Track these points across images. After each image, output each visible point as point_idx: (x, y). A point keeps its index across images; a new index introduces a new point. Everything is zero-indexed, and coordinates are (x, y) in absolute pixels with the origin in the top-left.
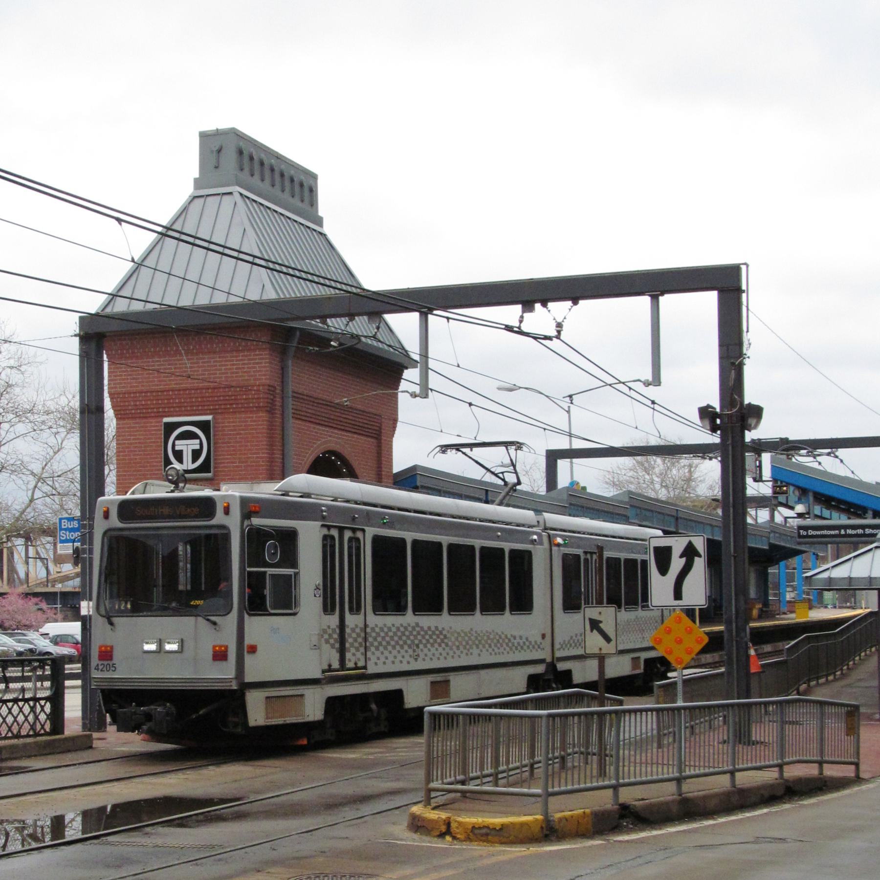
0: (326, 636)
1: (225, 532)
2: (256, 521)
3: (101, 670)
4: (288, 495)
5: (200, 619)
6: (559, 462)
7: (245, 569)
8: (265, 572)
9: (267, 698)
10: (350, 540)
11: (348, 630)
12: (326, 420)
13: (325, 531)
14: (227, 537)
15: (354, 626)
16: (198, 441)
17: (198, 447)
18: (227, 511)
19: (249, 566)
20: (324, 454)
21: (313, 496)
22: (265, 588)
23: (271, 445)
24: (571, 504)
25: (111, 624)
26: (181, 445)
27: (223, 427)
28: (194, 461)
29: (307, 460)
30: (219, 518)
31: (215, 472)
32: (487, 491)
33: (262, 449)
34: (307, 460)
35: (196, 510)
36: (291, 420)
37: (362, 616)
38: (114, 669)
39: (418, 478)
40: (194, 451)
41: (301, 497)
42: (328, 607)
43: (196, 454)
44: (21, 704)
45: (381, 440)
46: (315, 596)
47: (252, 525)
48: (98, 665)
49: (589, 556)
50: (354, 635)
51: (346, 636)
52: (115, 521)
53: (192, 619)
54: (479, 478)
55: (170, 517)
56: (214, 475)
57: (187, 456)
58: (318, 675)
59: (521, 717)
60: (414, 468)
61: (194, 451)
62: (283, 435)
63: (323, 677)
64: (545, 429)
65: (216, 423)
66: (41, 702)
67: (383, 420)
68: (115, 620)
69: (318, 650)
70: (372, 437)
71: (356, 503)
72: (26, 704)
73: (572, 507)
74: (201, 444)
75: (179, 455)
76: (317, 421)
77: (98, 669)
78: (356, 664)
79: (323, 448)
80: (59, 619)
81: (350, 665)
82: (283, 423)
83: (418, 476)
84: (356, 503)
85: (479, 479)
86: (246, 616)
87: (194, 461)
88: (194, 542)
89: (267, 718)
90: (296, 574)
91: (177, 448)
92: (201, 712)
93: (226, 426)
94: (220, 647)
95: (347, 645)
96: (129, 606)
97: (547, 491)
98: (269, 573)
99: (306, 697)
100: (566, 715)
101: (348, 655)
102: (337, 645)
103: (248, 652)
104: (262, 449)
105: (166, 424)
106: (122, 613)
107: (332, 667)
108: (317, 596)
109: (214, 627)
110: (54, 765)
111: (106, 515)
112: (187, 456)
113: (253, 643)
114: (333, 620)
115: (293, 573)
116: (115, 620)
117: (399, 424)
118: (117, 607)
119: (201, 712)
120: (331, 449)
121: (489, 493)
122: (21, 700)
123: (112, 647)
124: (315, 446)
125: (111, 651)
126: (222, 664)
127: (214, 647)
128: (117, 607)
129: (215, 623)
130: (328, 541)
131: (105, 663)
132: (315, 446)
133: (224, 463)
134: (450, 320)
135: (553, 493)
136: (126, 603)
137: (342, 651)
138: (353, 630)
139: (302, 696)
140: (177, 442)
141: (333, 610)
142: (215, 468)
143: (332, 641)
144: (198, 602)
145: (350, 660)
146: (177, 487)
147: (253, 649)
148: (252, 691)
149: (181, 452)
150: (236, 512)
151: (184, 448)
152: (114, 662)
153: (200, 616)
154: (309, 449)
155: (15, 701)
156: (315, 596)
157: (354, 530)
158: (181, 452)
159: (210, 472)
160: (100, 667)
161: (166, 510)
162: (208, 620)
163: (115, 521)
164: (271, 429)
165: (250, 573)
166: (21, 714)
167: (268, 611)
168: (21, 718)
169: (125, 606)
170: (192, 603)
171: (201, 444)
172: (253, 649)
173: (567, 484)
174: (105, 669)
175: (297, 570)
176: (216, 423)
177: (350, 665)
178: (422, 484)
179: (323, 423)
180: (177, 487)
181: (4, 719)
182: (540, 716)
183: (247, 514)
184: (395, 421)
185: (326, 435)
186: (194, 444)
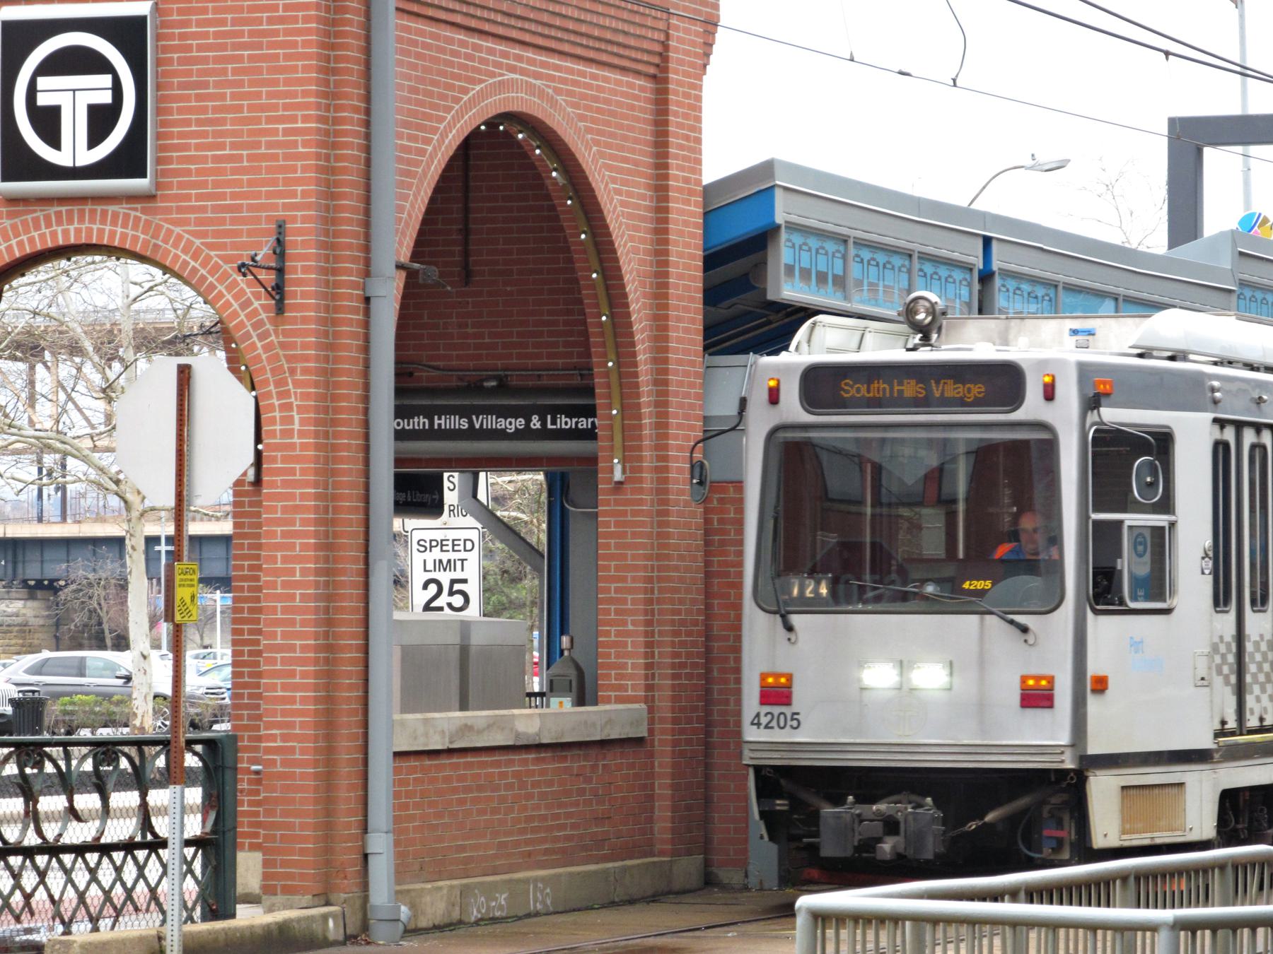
0: (1218, 659)
1: (1044, 436)
2: (1112, 415)
3: (767, 727)
4: (1151, 356)
5: (991, 620)
6: (1208, 152)
7: (1088, 517)
8: (1121, 522)
9: (1123, 788)
10: (1253, 447)
11: (1249, 647)
12: (499, 18)
13: (1217, 434)
14: (1050, 447)
15: (1258, 639)
16: (106, 80)
17: (106, 98)
18: (1049, 393)
19: (1096, 510)
20: (492, 123)
21: (1192, 357)
22: (1120, 556)
23: (330, 94)
24: (1243, 284)
25: (789, 628)
26: (53, 90)
27: (183, 36)
28: (94, 140)
29: (441, 141)
30: (1032, 407)
31: (157, 174)
32: (987, 241)
33: (305, 106)
34: (441, 141)
35: (977, 390)
36: (393, 19)
37: (1232, 616)
38: (795, 723)
39: (779, 198)
40: (94, 111)
41: (1215, 363)
42: (1220, 599)
43: (101, 120)
44: (141, 854)
45: (666, 80)
46: (1203, 573)
47: (1102, 423)
48: (758, 715)
49: (1229, 435)
50: (1258, 657)
51: (1247, 659)
52: (793, 409)
53: (974, 618)
54: (963, 202)
55: (922, 403)
56: (158, 185)
57: (74, 126)
58: (1205, 741)
59: (1093, 927)
60: (767, 168)
61: (94, 111)
62: (368, 64)
63: (1215, 746)
64: (1167, 54)
65: (164, 25)
66: (88, 856)
67: (674, 21)
68: (796, 619)
69: (1207, 690)
70: (638, 73)
71: (1251, 367)
72: (105, 860)
73: (1248, 293)
74: (117, 88)
75: (47, 122)
76: (473, 23)
77: (759, 724)
78: (1261, 719)
79: (493, 105)
80: (86, 642)
81: (1253, 722)
82: (367, 26)
83: (779, 194)
84: (1251, 367)
85: (965, 204)
86: (1090, 614)
87: (94, 140)
88: (984, 456)
89: (1124, 832)
90: (1172, 525)
91: (43, 100)
92: (989, 817)
93: (195, 36)
94: (1038, 678)
95: (1248, 679)
96: (824, 591)
97: (1172, 244)
98: (1127, 523)
99: (1189, 788)
100: (1234, 925)
101: (1250, 701)
102: (1233, 679)
103: (1094, 691)
104: (305, 106)
105: (9, 26)
106: (812, 606)
107: (1265, 723)
108: (1207, 572)
109: (1024, 637)
110: (718, 921)
111: (774, 397)
112: (74, 126)
113: (1101, 673)
114: (1227, 622)
115: (1165, 524)
116: (796, 619)
117: (721, 34)
118: (795, 592)
119: (989, 817)
120: (515, 107)
121: (995, 245)
122: (141, 846)
123: (790, 677)
124: (466, 98)
125: (789, 686)
126: (1038, 716)
127: (1024, 679)
128: (795, 592)
129: (1024, 630)
130: (1220, 449)
131: (776, 710)
132: (466, 98)
133: (185, 147)
134: (1170, 57)
135: (1187, 251)
136: (818, 583)
137: (1240, 691)
138: (1257, 644)
139: (1181, 785)
140: (43, 82)
141: (1227, 602)
142: (159, 161)
143: (1226, 670)
144: (980, 585)
145: (1252, 713)
146: (926, 340)
147: (1101, 685)
148: (1098, 772)
149: (55, 111)
150: (1069, 394)
151: (63, 100)
152: (795, 708)
153: (991, 613)
154: (448, 109)
155: (129, 847)
156: (1203, 573)
157: (1258, 428)
158: (55, 111)
159: (144, 176)
160: (764, 720)
161: (951, 389)
162: (1012, 622)
163: (793, 409)
164: (333, 47)
165: (1097, 524)
166: (41, 887)
167: (1122, 602)
168: (94, 893)
169: (816, 591)
170: (966, 585)
171: (117, 88)
172: (1101, 685)
173: (1232, 223)
174: (774, 723)
175: (1172, 518)
176: (164, 25)
177: (1253, 722)
178: (794, 218)
179: (487, 27)
180: (926, 340)
181: (6, 899)
182: (1153, 928)
183: (1092, 402)
184: (711, 25)
185: (498, 65)
186: (96, 89)
